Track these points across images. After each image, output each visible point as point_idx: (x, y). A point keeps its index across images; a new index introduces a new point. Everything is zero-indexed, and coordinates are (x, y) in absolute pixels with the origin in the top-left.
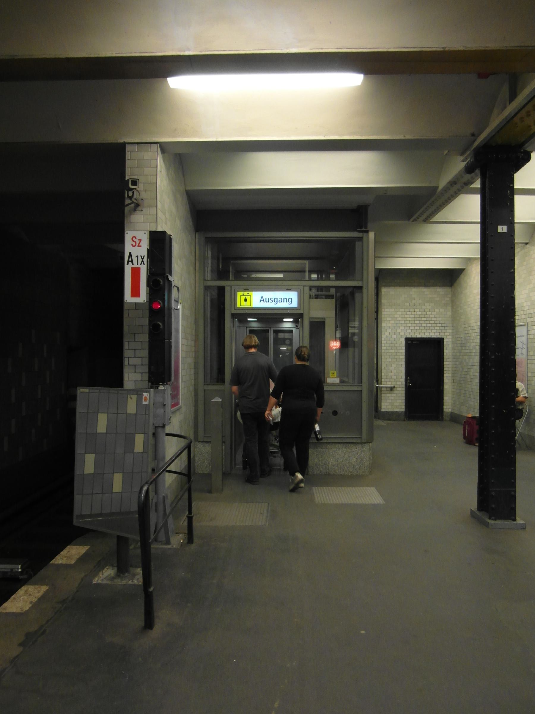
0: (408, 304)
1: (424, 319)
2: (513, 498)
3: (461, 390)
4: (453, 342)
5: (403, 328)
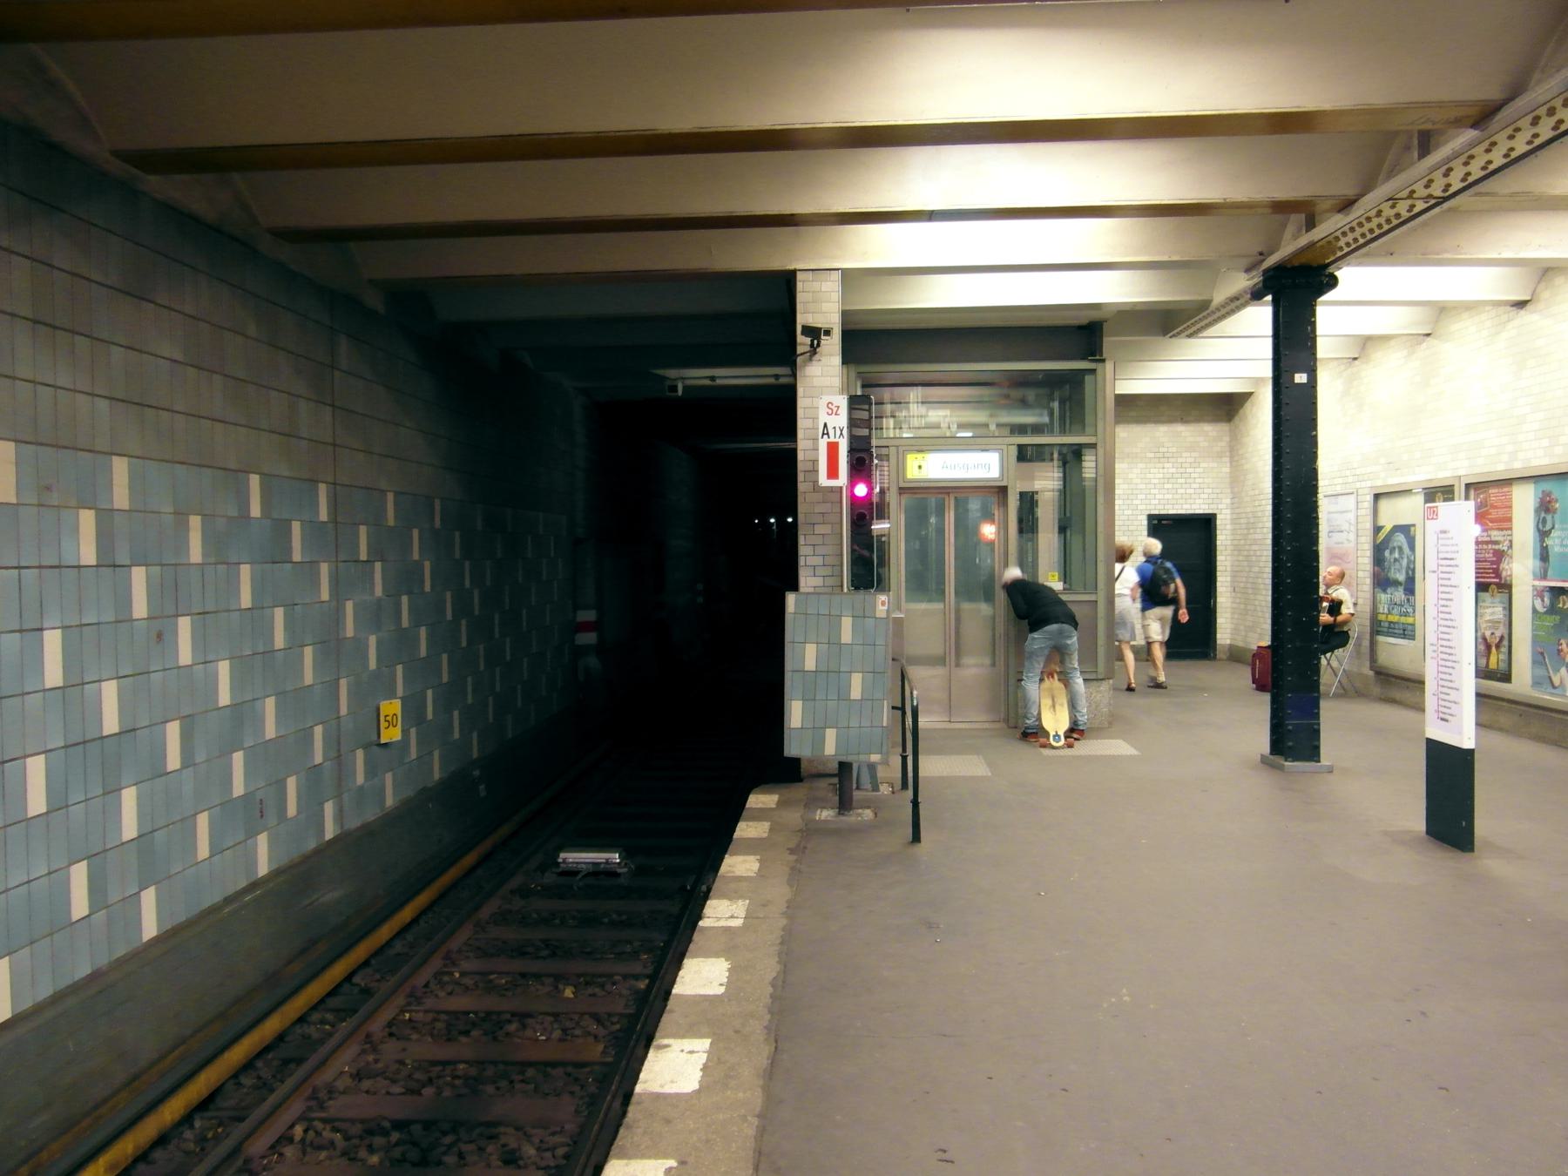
2: (1316, 733)
3: (1243, 610)
4: (1234, 521)
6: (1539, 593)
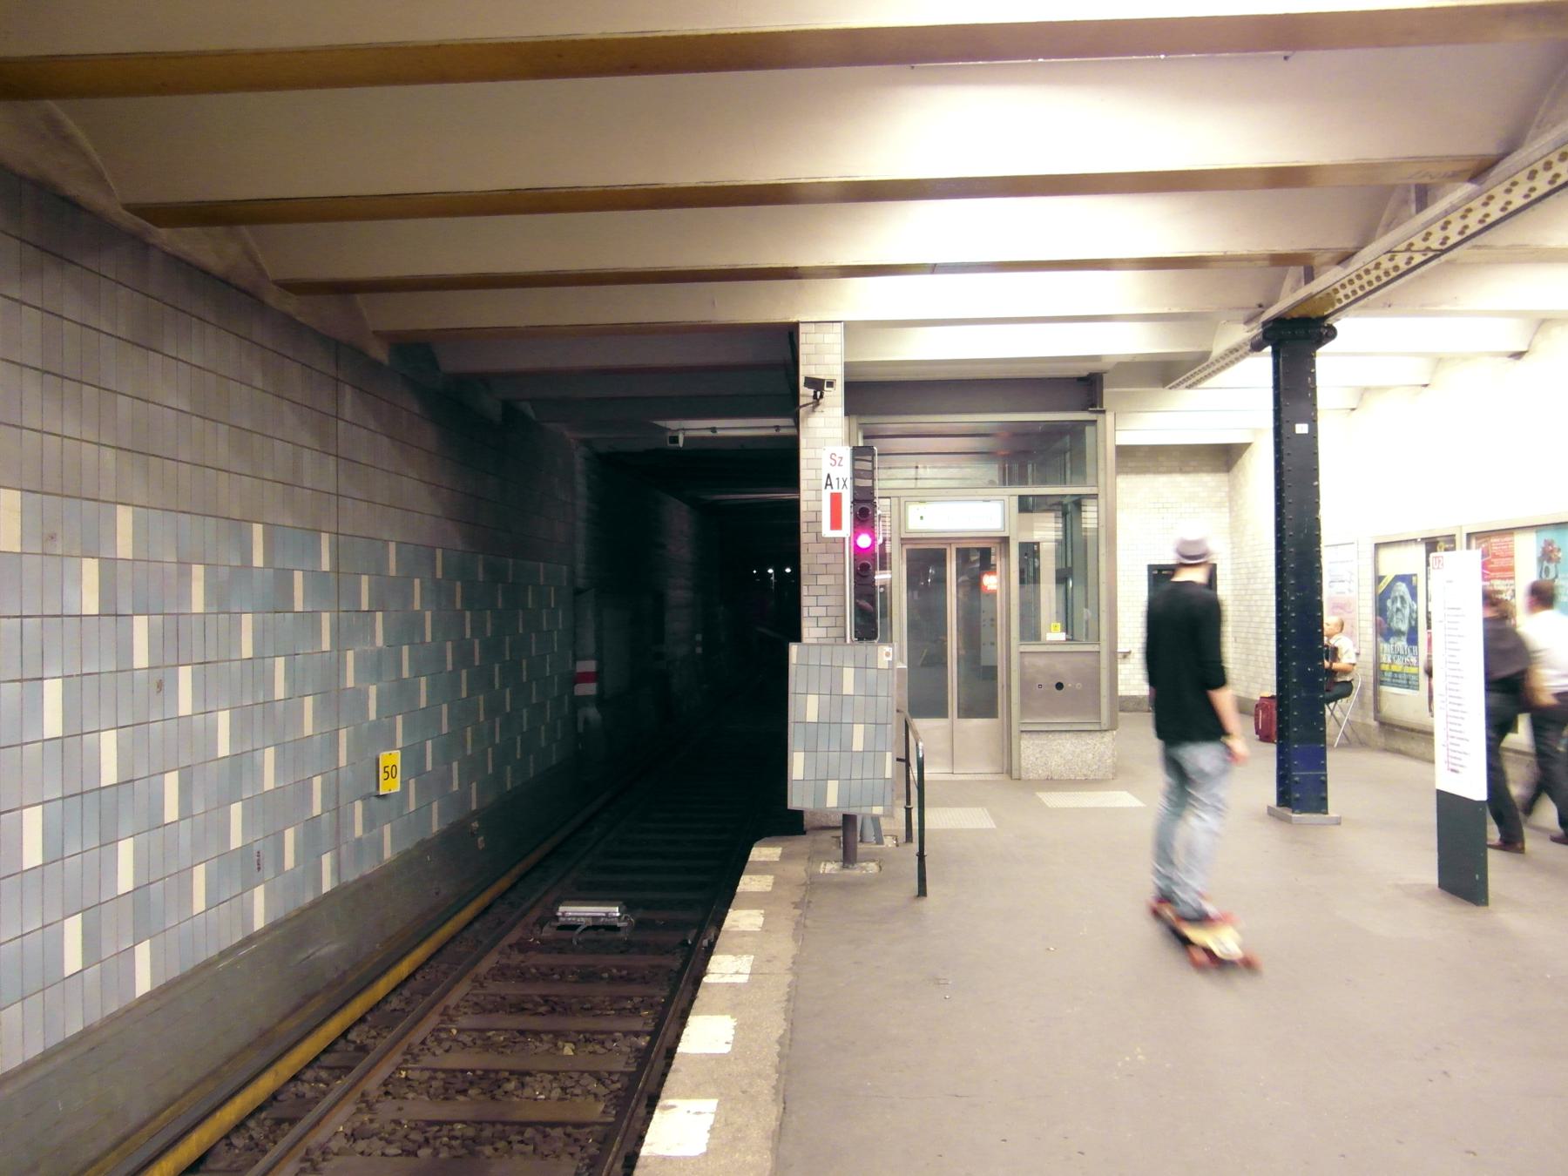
3: (1250, 660)
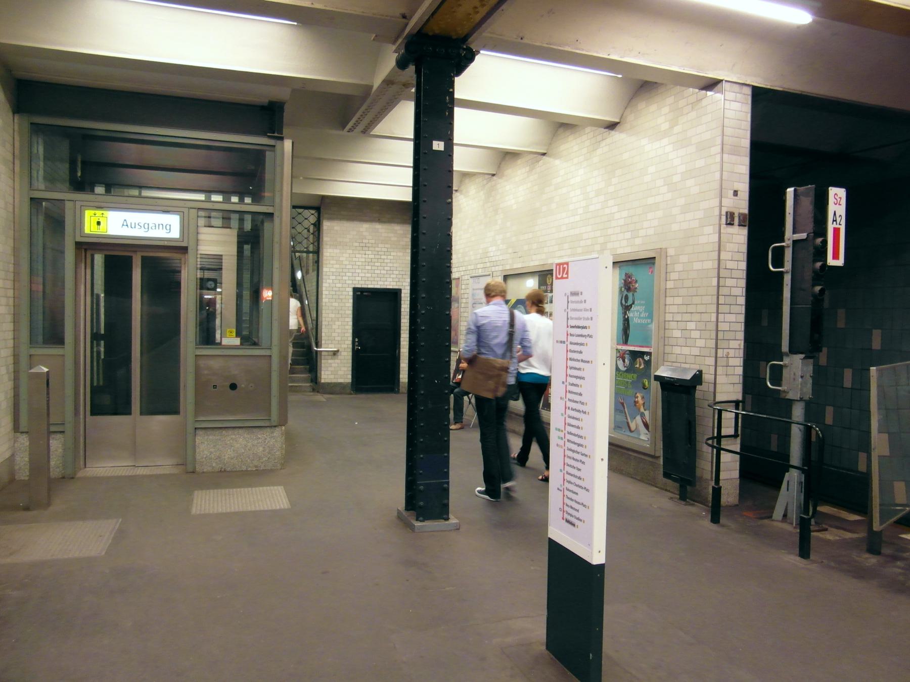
0: (357, 244)
1: (376, 264)
5: (350, 274)
6: (621, 356)
